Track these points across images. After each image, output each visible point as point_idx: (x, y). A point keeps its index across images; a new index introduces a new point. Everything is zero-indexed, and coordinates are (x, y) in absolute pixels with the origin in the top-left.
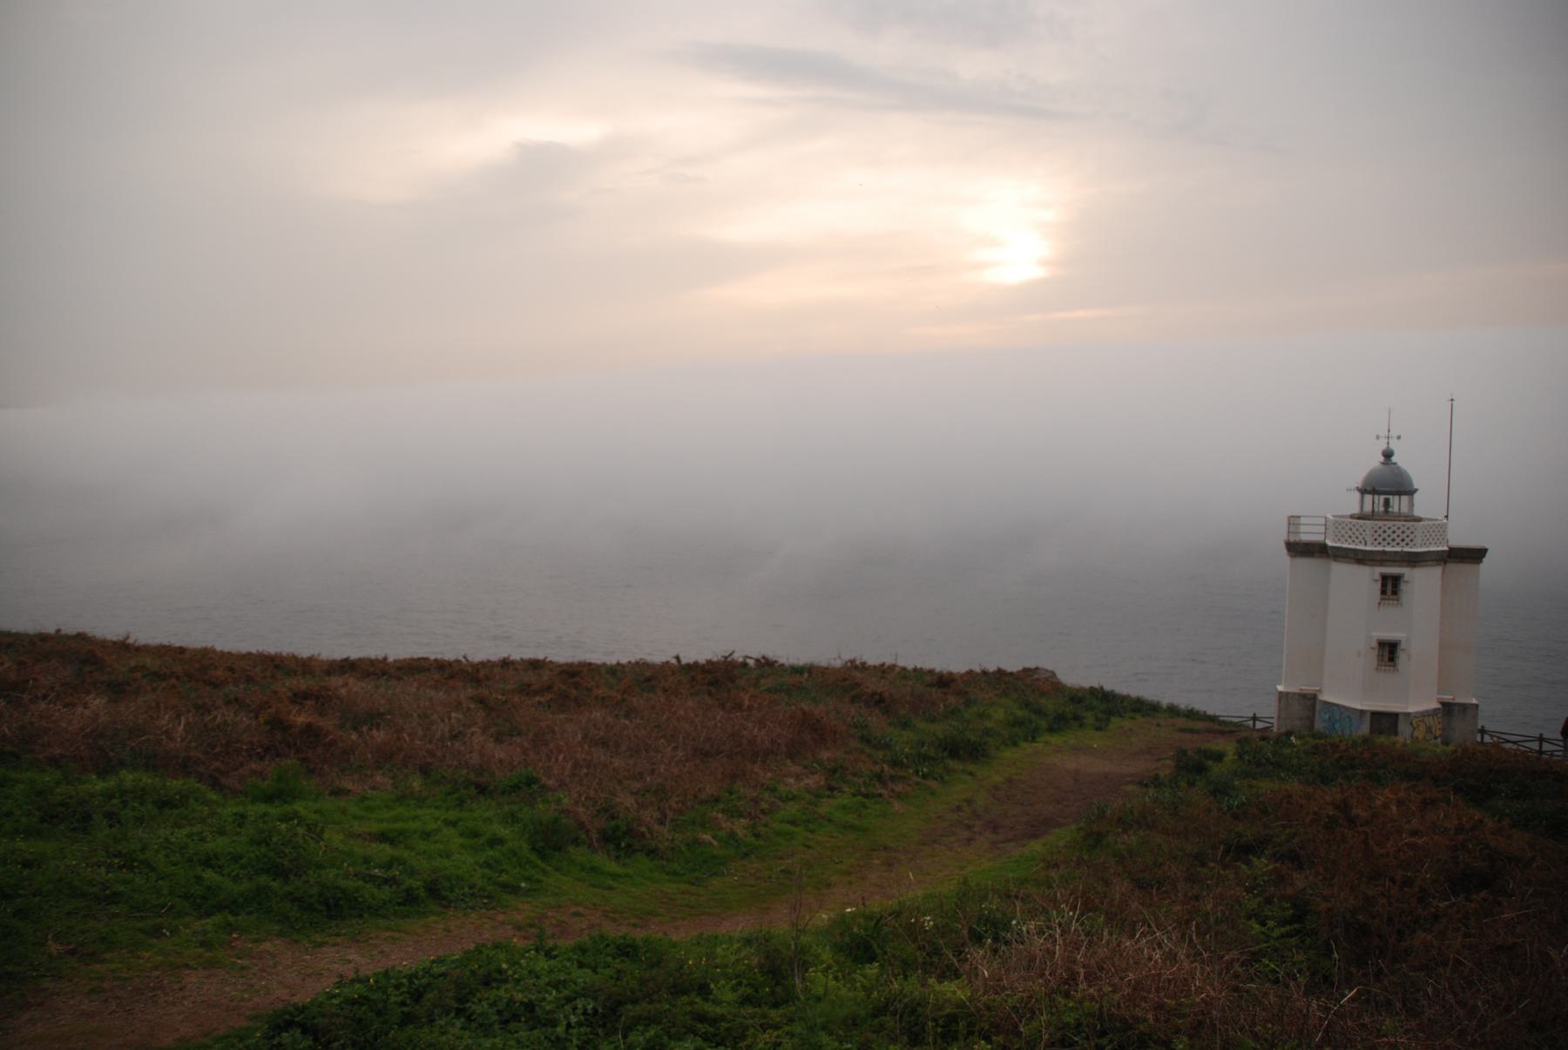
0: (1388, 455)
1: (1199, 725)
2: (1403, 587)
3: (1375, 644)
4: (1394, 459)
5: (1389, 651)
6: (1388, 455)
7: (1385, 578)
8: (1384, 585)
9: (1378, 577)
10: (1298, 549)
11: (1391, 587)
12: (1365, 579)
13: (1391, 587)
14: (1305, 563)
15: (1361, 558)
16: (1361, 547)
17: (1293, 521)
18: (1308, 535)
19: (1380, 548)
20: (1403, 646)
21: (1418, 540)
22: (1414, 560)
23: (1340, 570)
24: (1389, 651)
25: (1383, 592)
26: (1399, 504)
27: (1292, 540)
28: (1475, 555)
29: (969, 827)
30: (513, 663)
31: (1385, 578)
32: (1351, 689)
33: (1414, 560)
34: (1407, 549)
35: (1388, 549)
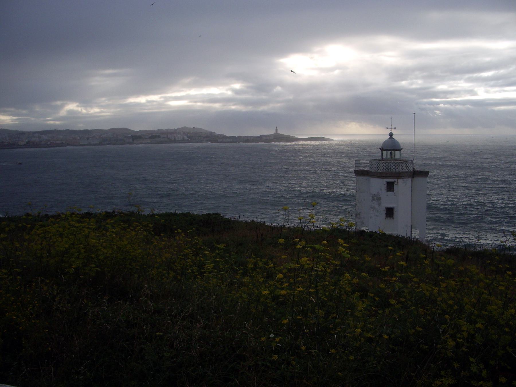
0: (391, 135)
3: (385, 209)
4: (393, 137)
5: (390, 212)
6: (391, 135)
9: (385, 183)
10: (359, 173)
11: (390, 187)
13: (390, 187)
14: (361, 178)
15: (380, 176)
17: (357, 163)
18: (364, 167)
20: (395, 210)
24: (390, 212)
26: (397, 154)
27: (356, 169)
28: (425, 174)
29: (315, 172)
30: (230, 225)
32: (374, 223)
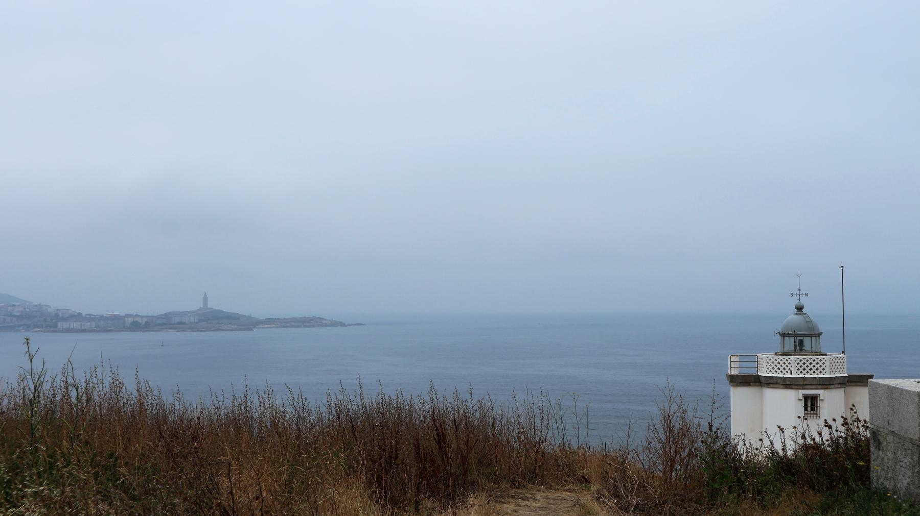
1: (66, 325)
2: (820, 404)
4: (804, 311)
7: (806, 397)
8: (806, 404)
9: (801, 397)
12: (792, 400)
13: (811, 403)
16: (788, 375)
19: (802, 376)
21: (827, 369)
22: (827, 384)
23: (772, 395)
25: (806, 409)
31: (806, 397)
33: (827, 384)
34: (821, 376)
35: (807, 376)
